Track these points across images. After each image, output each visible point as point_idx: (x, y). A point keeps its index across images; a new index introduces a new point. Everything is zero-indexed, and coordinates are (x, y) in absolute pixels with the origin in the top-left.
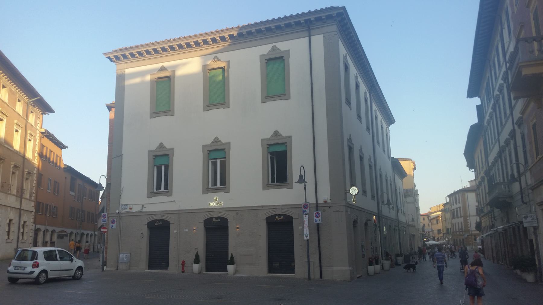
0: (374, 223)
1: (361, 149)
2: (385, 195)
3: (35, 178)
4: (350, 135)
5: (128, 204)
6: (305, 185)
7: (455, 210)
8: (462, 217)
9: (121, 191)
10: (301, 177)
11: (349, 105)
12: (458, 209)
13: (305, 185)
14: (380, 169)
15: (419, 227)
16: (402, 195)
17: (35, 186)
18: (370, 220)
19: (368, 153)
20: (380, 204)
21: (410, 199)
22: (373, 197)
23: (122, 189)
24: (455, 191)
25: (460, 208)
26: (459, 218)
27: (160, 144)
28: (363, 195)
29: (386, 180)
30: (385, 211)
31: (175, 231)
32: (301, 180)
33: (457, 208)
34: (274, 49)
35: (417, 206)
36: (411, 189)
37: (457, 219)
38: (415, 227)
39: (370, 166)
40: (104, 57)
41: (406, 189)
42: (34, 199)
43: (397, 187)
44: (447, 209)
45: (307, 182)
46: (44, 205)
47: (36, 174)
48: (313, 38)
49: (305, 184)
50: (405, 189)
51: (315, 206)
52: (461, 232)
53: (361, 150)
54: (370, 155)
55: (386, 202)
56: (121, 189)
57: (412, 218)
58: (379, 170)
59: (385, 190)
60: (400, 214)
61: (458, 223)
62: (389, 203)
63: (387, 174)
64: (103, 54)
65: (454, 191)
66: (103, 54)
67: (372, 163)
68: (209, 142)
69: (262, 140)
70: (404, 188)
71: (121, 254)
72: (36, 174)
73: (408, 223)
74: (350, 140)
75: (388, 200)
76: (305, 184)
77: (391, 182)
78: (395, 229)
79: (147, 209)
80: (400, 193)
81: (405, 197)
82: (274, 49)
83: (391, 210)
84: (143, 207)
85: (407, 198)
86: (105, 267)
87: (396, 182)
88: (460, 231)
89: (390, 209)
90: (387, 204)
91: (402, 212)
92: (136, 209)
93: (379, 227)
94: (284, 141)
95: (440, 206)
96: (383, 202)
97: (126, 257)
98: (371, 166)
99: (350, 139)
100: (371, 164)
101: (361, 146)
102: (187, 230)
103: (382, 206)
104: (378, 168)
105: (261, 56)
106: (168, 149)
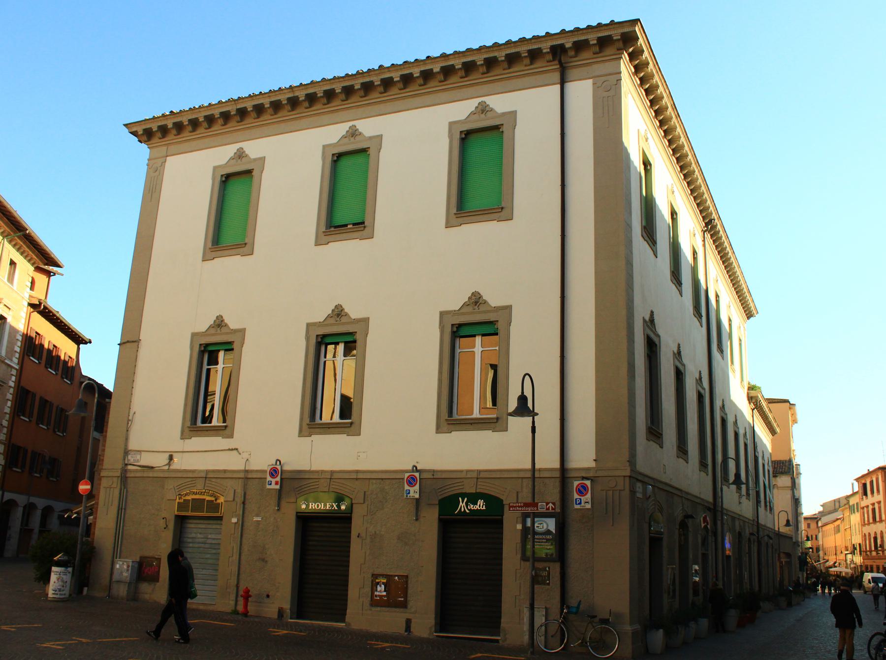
0: (703, 525)
1: (679, 353)
2: (732, 464)
3: (10, 397)
4: (652, 312)
5: (140, 451)
6: (533, 422)
7: (871, 507)
8: (884, 522)
9: (130, 420)
10: (522, 399)
11: (651, 245)
12: (876, 506)
13: (533, 422)
14: (723, 406)
15: (631, 631)
16: (769, 471)
17: (9, 412)
18: (691, 517)
19: (694, 364)
20: (720, 484)
21: (784, 481)
22: (703, 465)
23: (131, 414)
24: (870, 470)
25: (879, 503)
26: (878, 524)
27: (217, 317)
28: (678, 457)
29: (736, 435)
30: (731, 498)
31: (234, 520)
32: (524, 408)
33: (873, 504)
34: (483, 109)
35: (797, 497)
36: (786, 461)
37: (873, 525)
38: (792, 538)
39: (700, 397)
40: (126, 130)
41: (778, 461)
42: (4, 439)
43: (758, 453)
44: (853, 505)
45: (537, 414)
46: (29, 455)
47: (12, 388)
48: (572, 87)
49: (533, 419)
50: (775, 461)
51: (558, 474)
52: (881, 552)
53: (678, 354)
54: (700, 372)
55: (732, 478)
56: (130, 418)
57: (787, 519)
58: (720, 408)
59: (731, 453)
60: (762, 510)
61: (869, 534)
62: (738, 481)
63: (738, 421)
64: (125, 125)
65: (868, 470)
66: (125, 125)
67: (704, 389)
68: (320, 317)
69: (442, 314)
70: (773, 459)
71: (119, 562)
72: (12, 388)
73: (779, 528)
74: (650, 323)
75: (738, 475)
76: (533, 419)
77: (747, 439)
78: (749, 539)
79: (179, 463)
80: (764, 465)
81: (775, 476)
82: (483, 109)
83: (744, 499)
84: (171, 458)
85: (778, 479)
86: (86, 589)
87: (756, 440)
88: (880, 551)
89: (740, 496)
90: (733, 483)
91: (766, 506)
92: (159, 461)
93: (715, 534)
94: (491, 317)
95: (839, 502)
96: (725, 478)
97: (128, 570)
98: (702, 396)
99: (652, 320)
100: (702, 391)
101: (679, 345)
102: (259, 519)
103: (725, 488)
104: (718, 404)
105: (451, 124)
106: (232, 330)
